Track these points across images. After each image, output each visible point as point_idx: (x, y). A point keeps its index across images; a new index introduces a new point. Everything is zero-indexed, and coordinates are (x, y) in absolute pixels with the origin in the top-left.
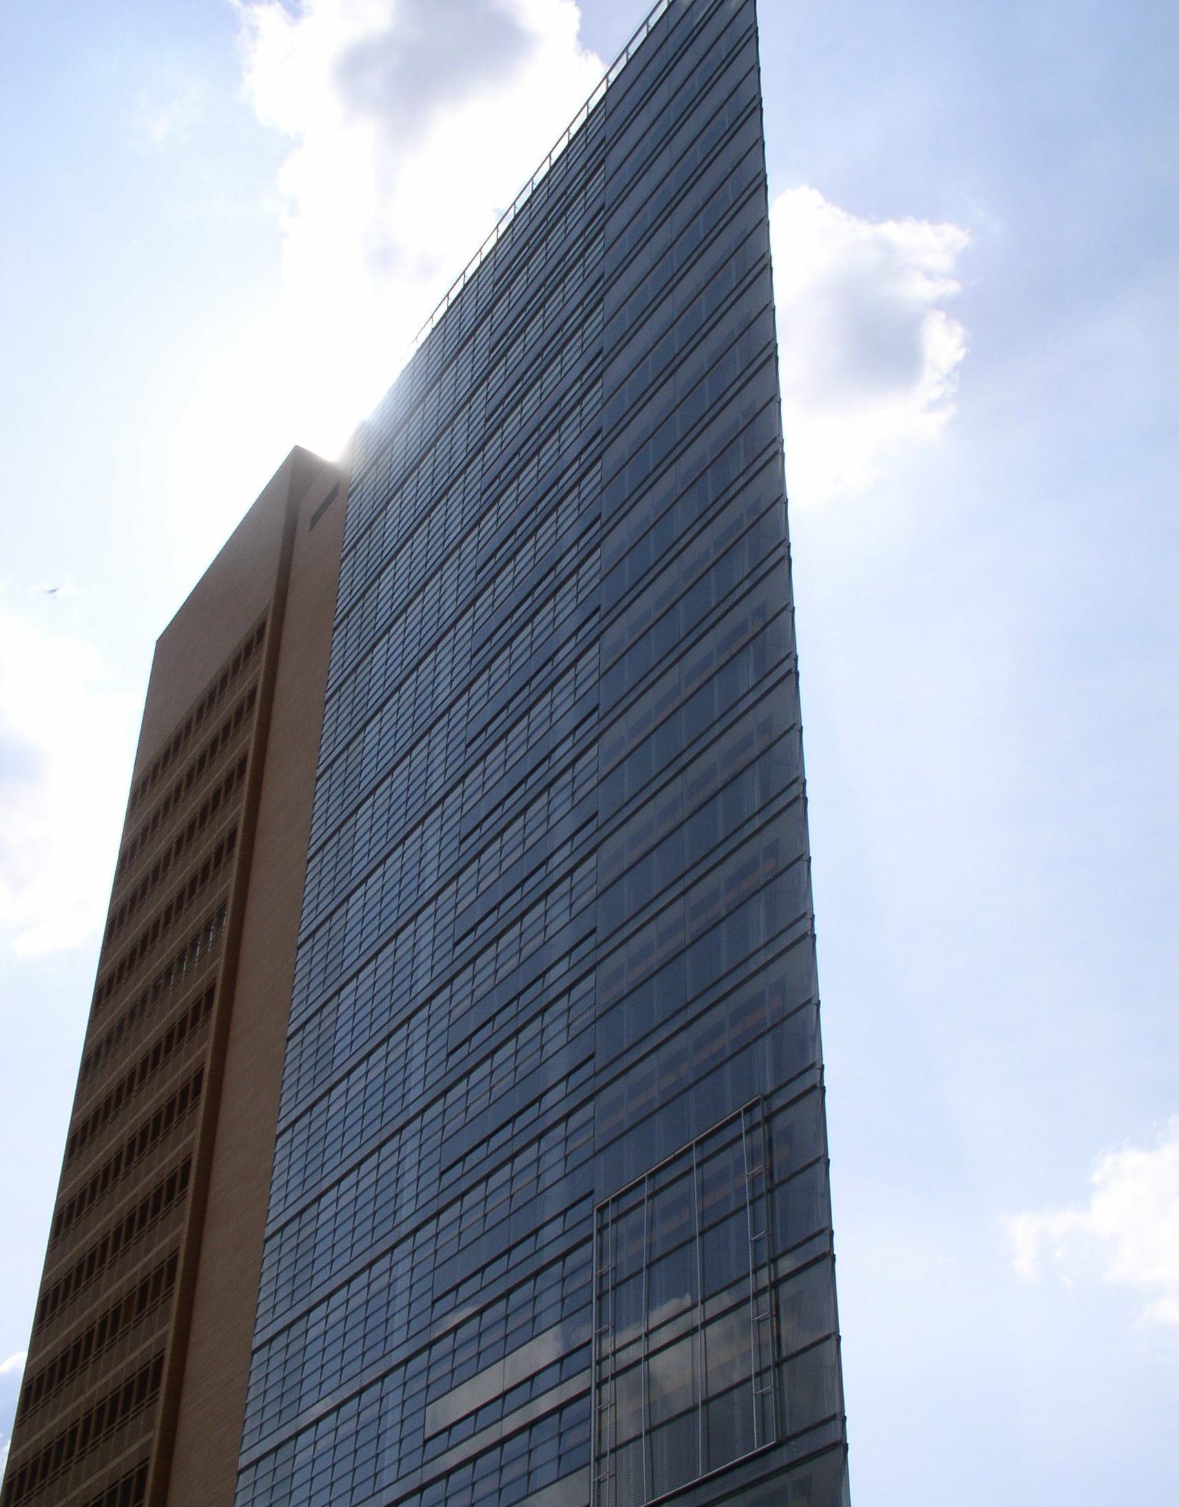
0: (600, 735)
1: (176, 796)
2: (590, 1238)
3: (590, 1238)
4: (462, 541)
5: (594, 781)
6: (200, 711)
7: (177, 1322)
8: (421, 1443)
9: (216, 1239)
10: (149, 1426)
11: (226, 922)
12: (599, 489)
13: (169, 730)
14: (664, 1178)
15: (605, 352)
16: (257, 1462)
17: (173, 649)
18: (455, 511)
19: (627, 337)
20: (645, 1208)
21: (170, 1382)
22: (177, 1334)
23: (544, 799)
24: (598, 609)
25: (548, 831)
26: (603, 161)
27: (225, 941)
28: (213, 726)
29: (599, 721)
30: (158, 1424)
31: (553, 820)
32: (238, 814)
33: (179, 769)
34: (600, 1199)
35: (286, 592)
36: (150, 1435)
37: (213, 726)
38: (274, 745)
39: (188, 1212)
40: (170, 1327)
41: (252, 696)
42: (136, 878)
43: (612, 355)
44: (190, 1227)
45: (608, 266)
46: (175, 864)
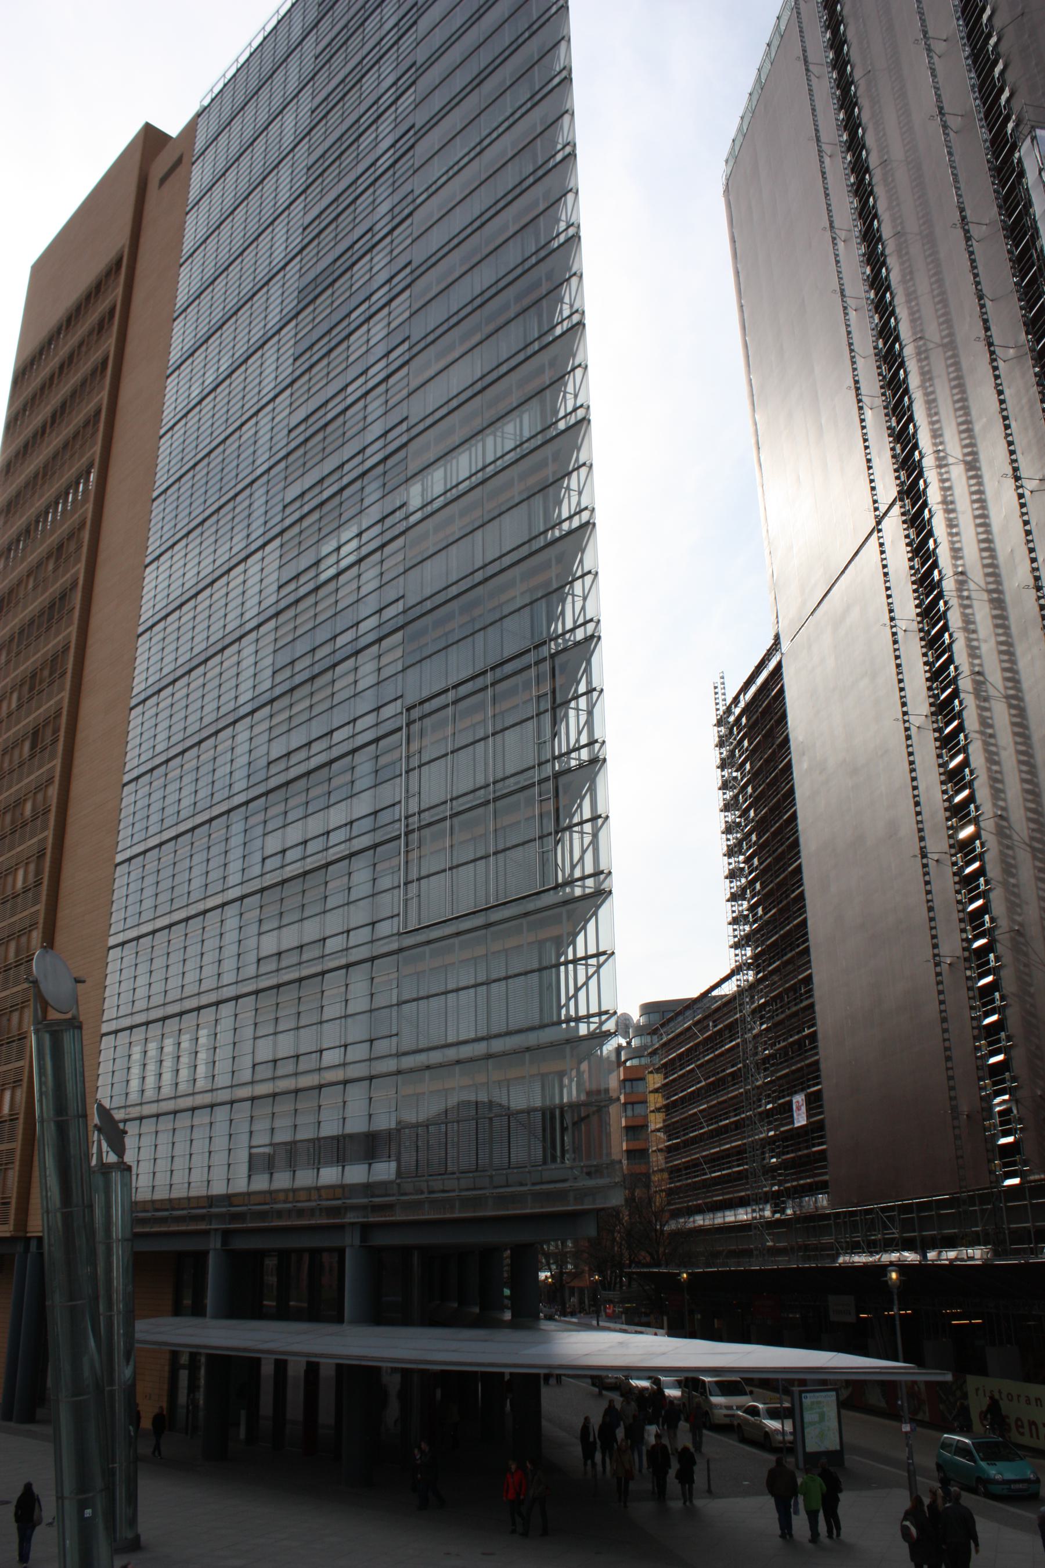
0: (413, 281)
1: (41, 432)
2: (400, 729)
3: (400, 729)
4: (281, 329)
5: (409, 241)
6: (69, 320)
7: (54, 830)
8: (266, 764)
9: (89, 705)
10: (62, 689)
11: (86, 535)
12: (413, 106)
13: (43, 333)
14: (463, 690)
15: (419, 5)
16: (137, 778)
17: (46, 272)
18: (293, 73)
19: (437, 54)
20: (450, 709)
21: (114, 367)
22: (71, 698)
23: (368, 257)
24: (410, 263)
25: (367, 351)
26: (415, 23)
27: (47, 869)
28: (79, 333)
29: (418, 10)
30: (44, 898)
31: (374, 271)
32: (109, 345)
33: (44, 412)
34: (409, 700)
35: (146, 179)
36: (62, 694)
37: (79, 333)
38: (131, 348)
39: (68, 686)
40: (73, 629)
41: (98, 413)
42: (20, 441)
43: (421, 427)
44: (60, 789)
45: (420, 118)
46: (50, 433)
